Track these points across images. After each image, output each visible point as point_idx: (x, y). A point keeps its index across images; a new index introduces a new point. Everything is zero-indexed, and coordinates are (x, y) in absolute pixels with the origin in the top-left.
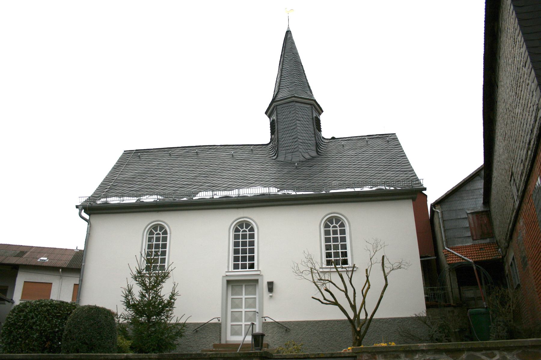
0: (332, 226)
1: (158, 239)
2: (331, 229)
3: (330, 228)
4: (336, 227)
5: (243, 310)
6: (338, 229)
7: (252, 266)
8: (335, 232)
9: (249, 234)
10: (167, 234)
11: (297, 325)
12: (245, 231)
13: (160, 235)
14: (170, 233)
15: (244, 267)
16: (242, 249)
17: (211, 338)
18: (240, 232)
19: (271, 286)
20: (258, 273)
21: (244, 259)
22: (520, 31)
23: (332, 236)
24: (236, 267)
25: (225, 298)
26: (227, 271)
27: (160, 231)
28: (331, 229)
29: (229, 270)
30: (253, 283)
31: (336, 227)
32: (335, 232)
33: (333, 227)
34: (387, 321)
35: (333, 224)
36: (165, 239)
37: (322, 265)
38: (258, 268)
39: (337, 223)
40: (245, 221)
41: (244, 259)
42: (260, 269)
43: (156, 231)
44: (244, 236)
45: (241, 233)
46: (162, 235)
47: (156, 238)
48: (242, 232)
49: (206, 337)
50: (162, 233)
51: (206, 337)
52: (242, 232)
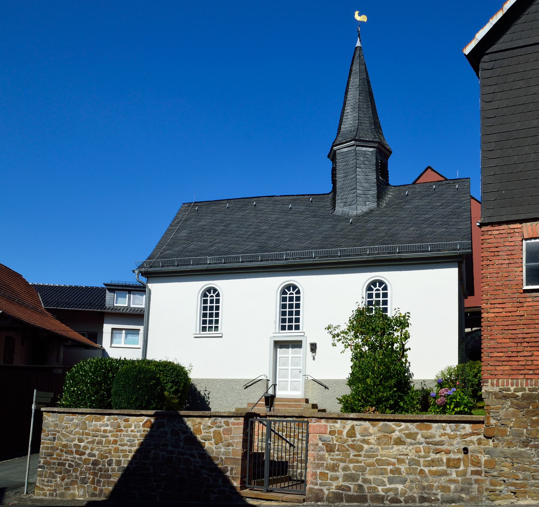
0: (375, 289)
1: (212, 301)
2: (209, 298)
3: (287, 295)
4: (293, 294)
5: (290, 368)
6: (295, 295)
7: (297, 328)
8: (378, 295)
9: (296, 297)
10: (299, 293)
11: (335, 383)
12: (292, 294)
13: (293, 294)
14: (223, 296)
15: (290, 328)
16: (209, 313)
17: (259, 392)
18: (373, 291)
19: (313, 347)
20: (302, 334)
21: (290, 320)
22: (488, 54)
23: (209, 305)
24: (283, 328)
25: (275, 356)
26: (274, 332)
27: (293, 290)
28: (209, 298)
29: (276, 331)
30: (297, 344)
31: (293, 294)
32: (378, 295)
33: (377, 290)
34: (418, 382)
35: (290, 291)
36: (218, 301)
37: (276, 331)
38: (221, 331)
39: (380, 286)
40: (291, 284)
41: (290, 320)
42: (222, 332)
43: (210, 293)
44: (291, 299)
45: (288, 296)
46: (216, 297)
47: (376, 294)
48: (290, 294)
49: (255, 392)
50: (295, 293)
51: (255, 392)
52: (290, 294)
